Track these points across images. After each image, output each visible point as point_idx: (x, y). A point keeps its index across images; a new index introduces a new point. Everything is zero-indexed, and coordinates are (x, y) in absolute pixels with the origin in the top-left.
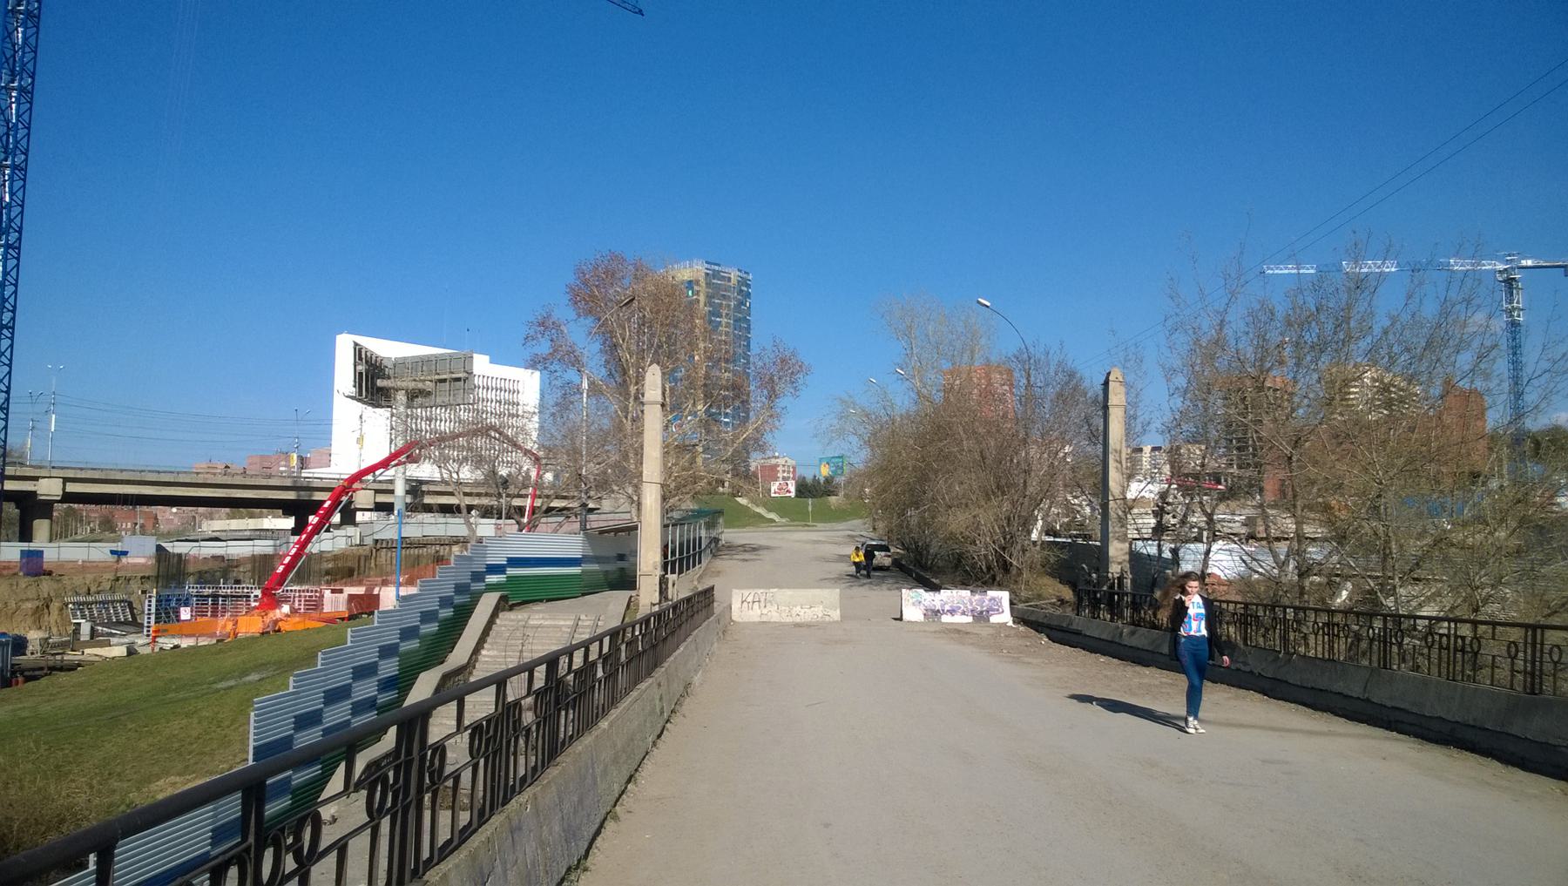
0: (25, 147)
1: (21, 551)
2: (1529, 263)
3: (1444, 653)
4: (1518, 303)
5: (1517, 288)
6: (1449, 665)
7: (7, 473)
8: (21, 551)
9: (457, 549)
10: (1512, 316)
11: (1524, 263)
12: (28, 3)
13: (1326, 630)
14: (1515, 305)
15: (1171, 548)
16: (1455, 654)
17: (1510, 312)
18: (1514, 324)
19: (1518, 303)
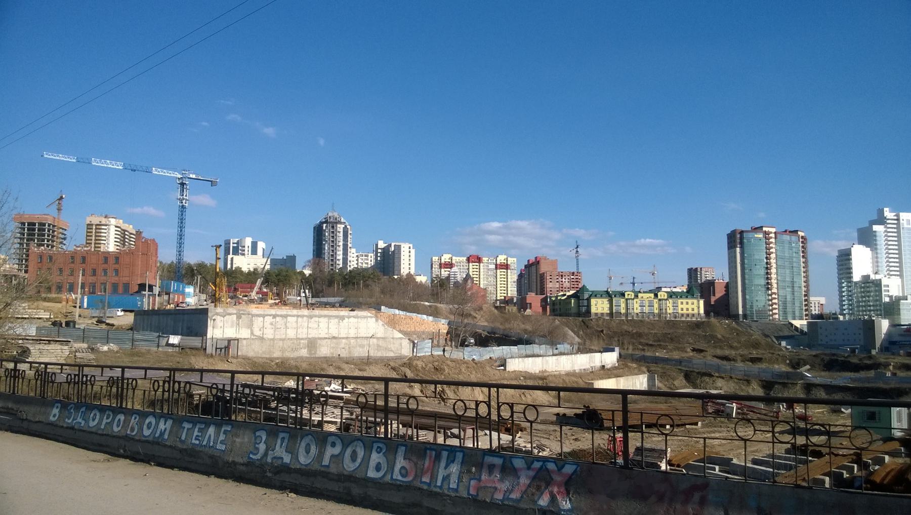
0: (753, 439)
1: (252, 254)
2: (194, 176)
3: (76, 385)
4: (186, 196)
5: (186, 188)
6: (82, 389)
7: (492, 389)
8: (252, 254)
9: (188, 300)
10: (182, 203)
11: (191, 176)
12: (910, 271)
13: (85, 379)
14: (184, 197)
15: (292, 259)
16: (82, 385)
17: (181, 200)
18: (183, 207)
19: (186, 196)
